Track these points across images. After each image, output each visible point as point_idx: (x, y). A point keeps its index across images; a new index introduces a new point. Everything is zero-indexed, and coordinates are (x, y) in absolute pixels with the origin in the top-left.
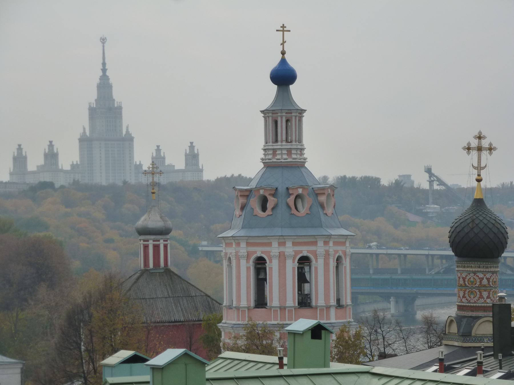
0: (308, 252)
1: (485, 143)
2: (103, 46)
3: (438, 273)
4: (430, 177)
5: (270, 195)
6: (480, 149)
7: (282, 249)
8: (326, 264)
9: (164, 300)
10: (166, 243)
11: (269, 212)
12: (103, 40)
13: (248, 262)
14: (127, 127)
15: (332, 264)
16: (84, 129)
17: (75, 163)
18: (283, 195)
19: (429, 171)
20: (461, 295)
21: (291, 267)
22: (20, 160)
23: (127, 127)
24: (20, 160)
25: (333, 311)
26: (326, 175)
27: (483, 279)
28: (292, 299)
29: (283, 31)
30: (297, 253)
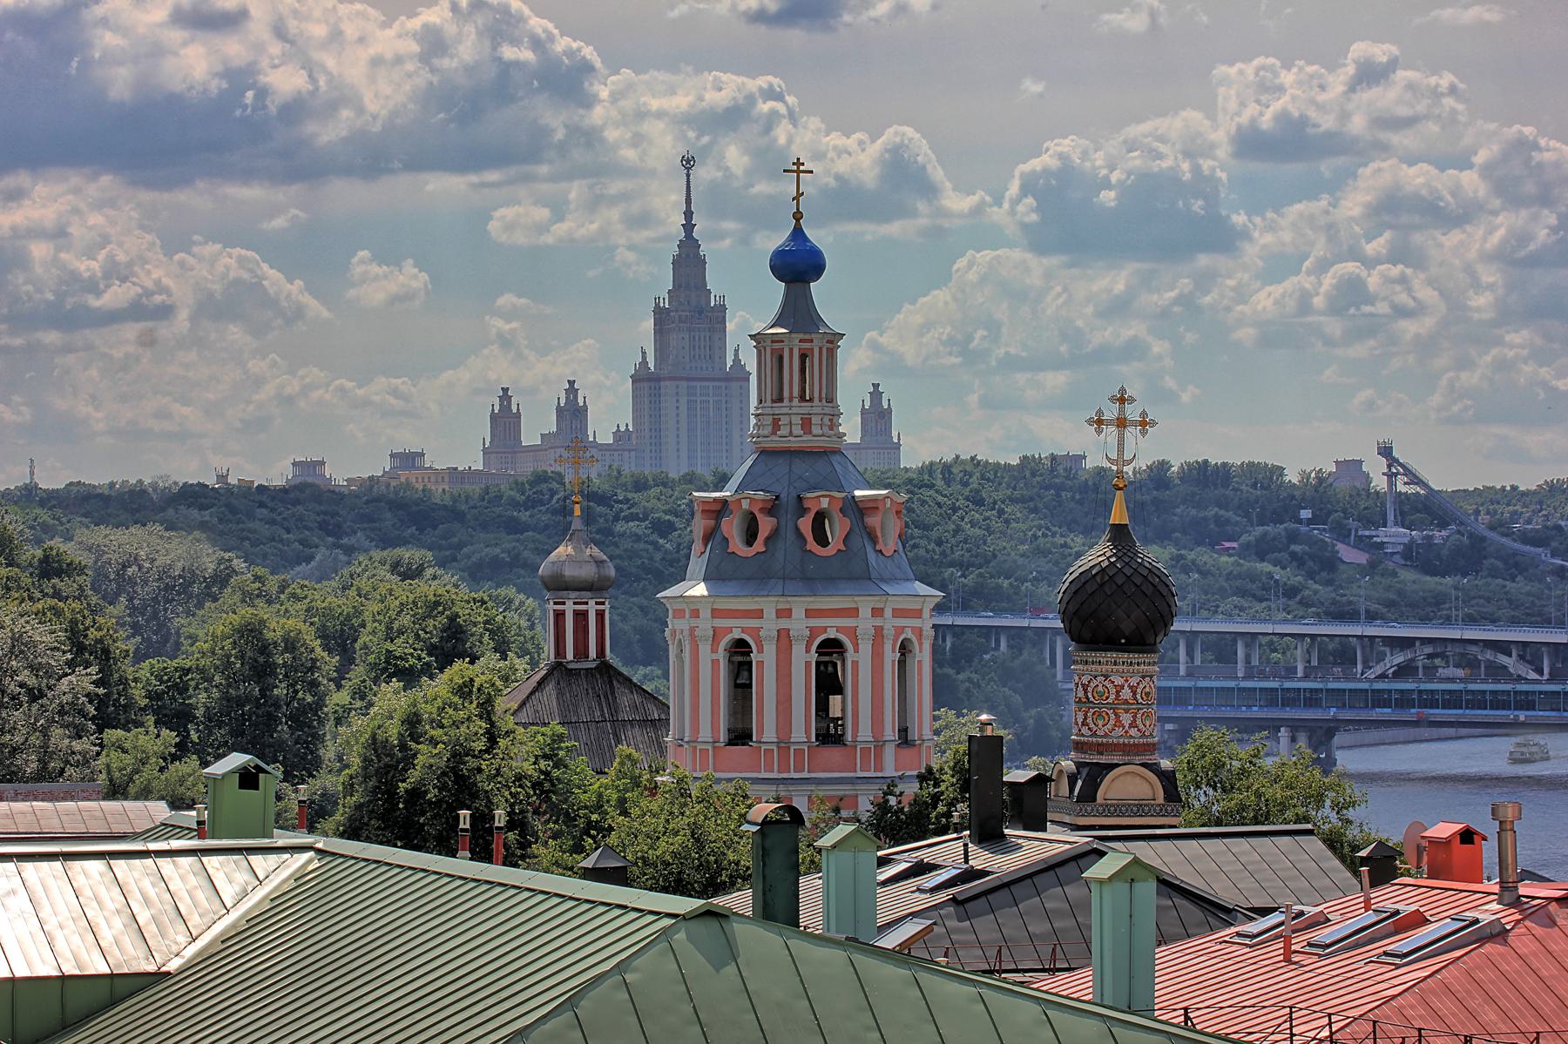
0: (839, 629)
2: (688, 175)
3: (1383, 676)
4: (1389, 466)
5: (761, 510)
6: (1121, 423)
7: (784, 623)
8: (877, 655)
9: (593, 726)
10: (601, 607)
11: (759, 546)
12: (688, 162)
13: (714, 650)
14: (737, 351)
15: (891, 656)
16: (644, 353)
17: (623, 429)
18: (1320, 480)
19: (1386, 451)
20: (1080, 721)
21: (803, 660)
22: (505, 420)
23: (737, 351)
24: (505, 420)
25: (889, 752)
26: (1167, 459)
27: (1122, 687)
28: (802, 728)
29: (798, 172)
30: (814, 632)
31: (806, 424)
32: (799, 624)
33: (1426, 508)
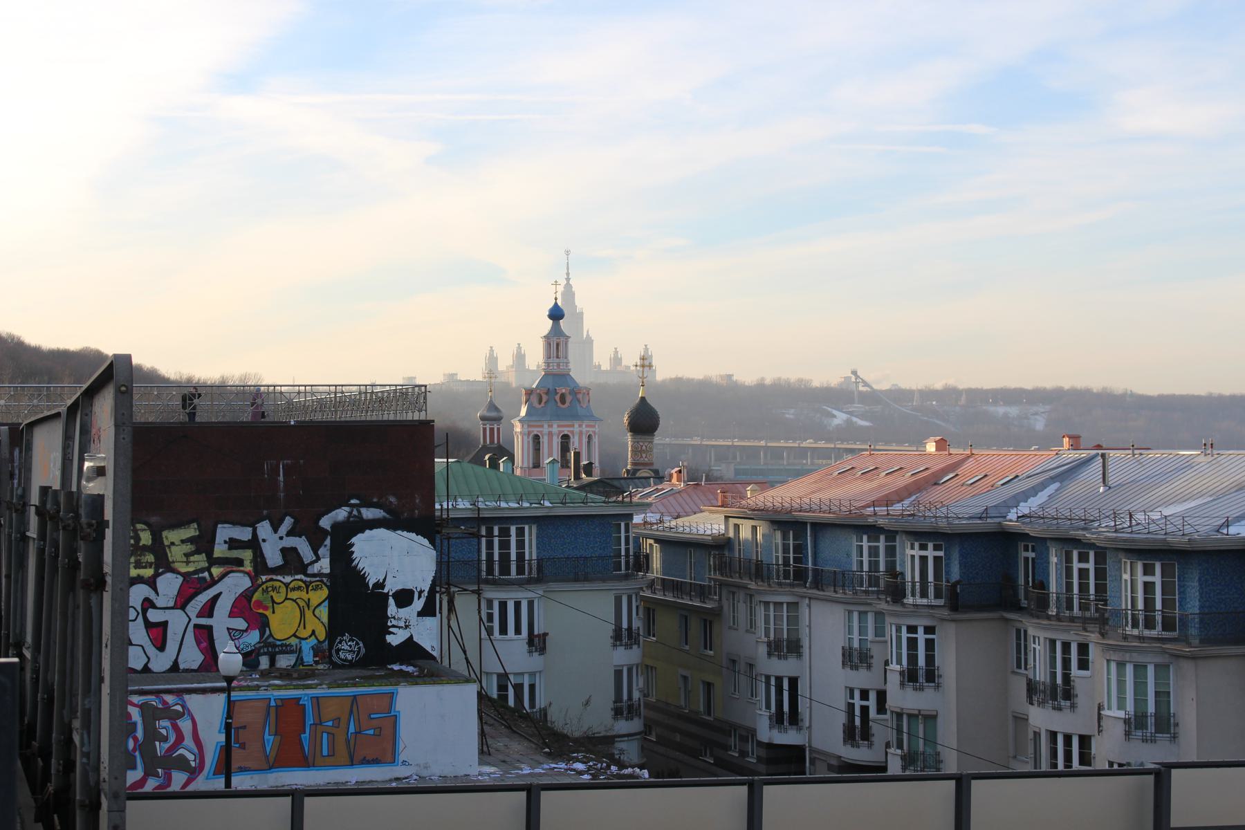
1: (647, 363)
11: (567, 404)
15: (585, 440)
21: (557, 441)
24: (492, 360)
31: (558, 365)
32: (555, 429)
33: (873, 397)
